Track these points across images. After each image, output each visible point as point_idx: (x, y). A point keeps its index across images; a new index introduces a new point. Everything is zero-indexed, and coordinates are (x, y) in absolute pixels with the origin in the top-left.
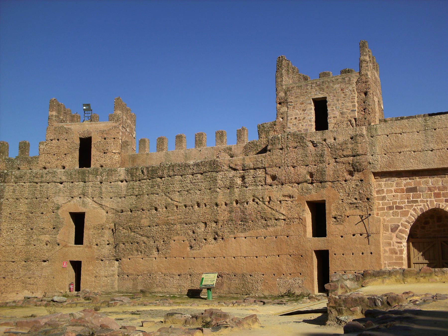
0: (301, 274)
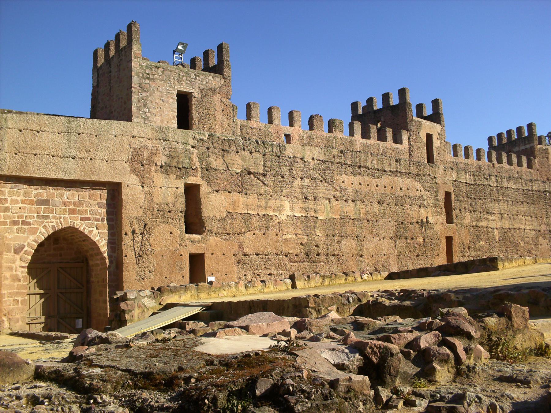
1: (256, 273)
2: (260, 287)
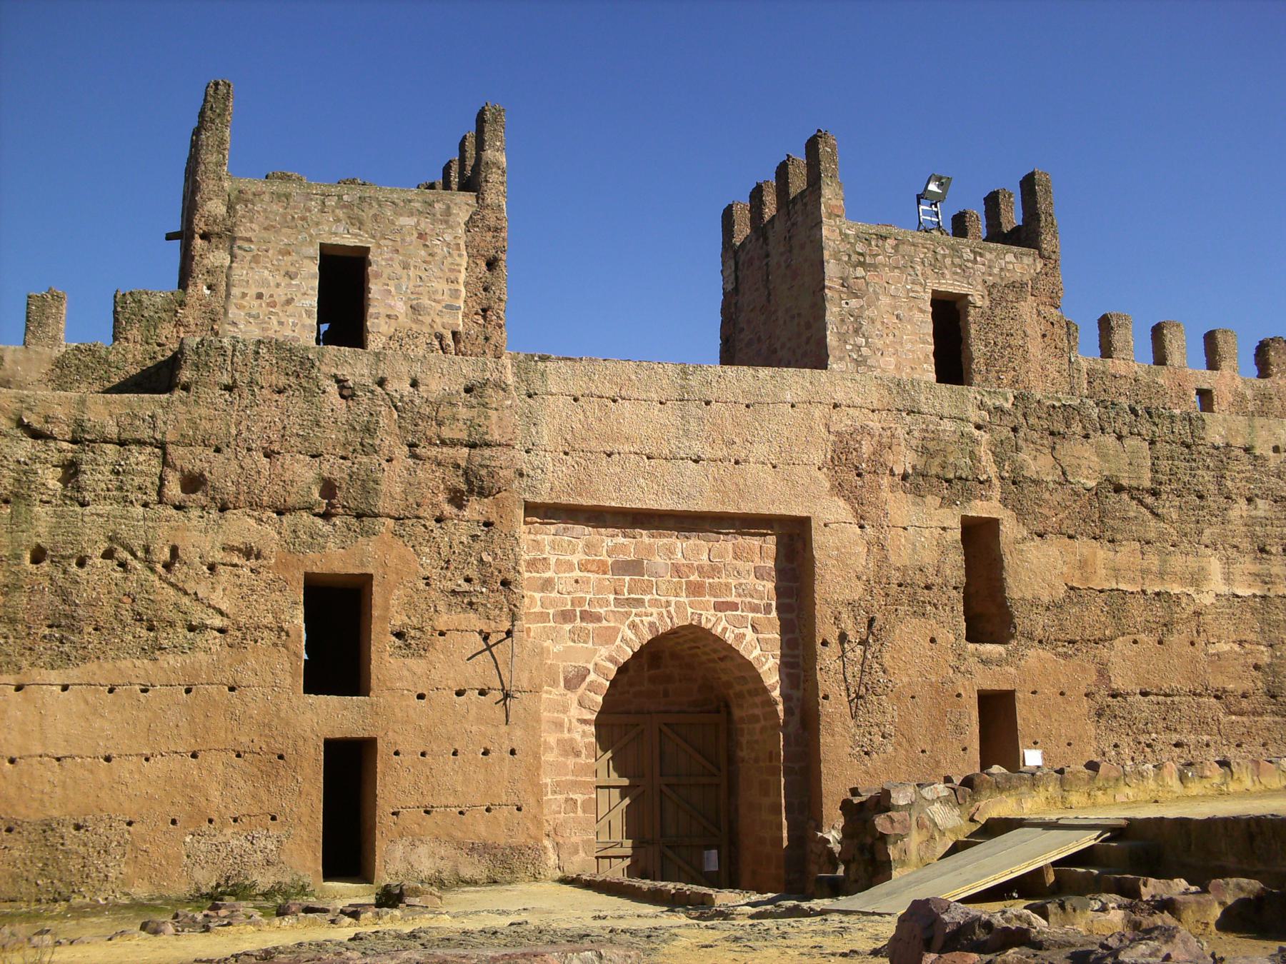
0: (274, 818)
1: (1142, 739)
2: (1217, 780)
